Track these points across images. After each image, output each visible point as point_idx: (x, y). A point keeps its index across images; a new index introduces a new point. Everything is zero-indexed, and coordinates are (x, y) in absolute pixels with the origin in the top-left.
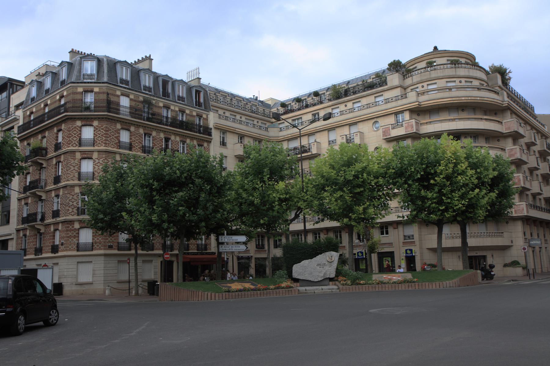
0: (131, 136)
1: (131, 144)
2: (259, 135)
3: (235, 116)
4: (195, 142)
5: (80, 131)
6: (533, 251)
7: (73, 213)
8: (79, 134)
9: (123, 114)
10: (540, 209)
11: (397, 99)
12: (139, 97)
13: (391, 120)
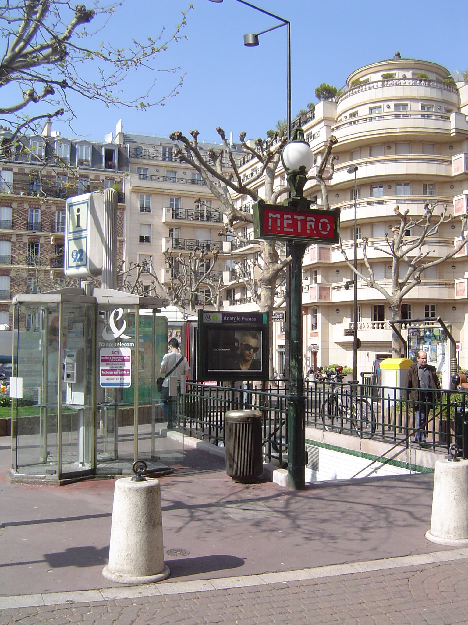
2: (204, 194)
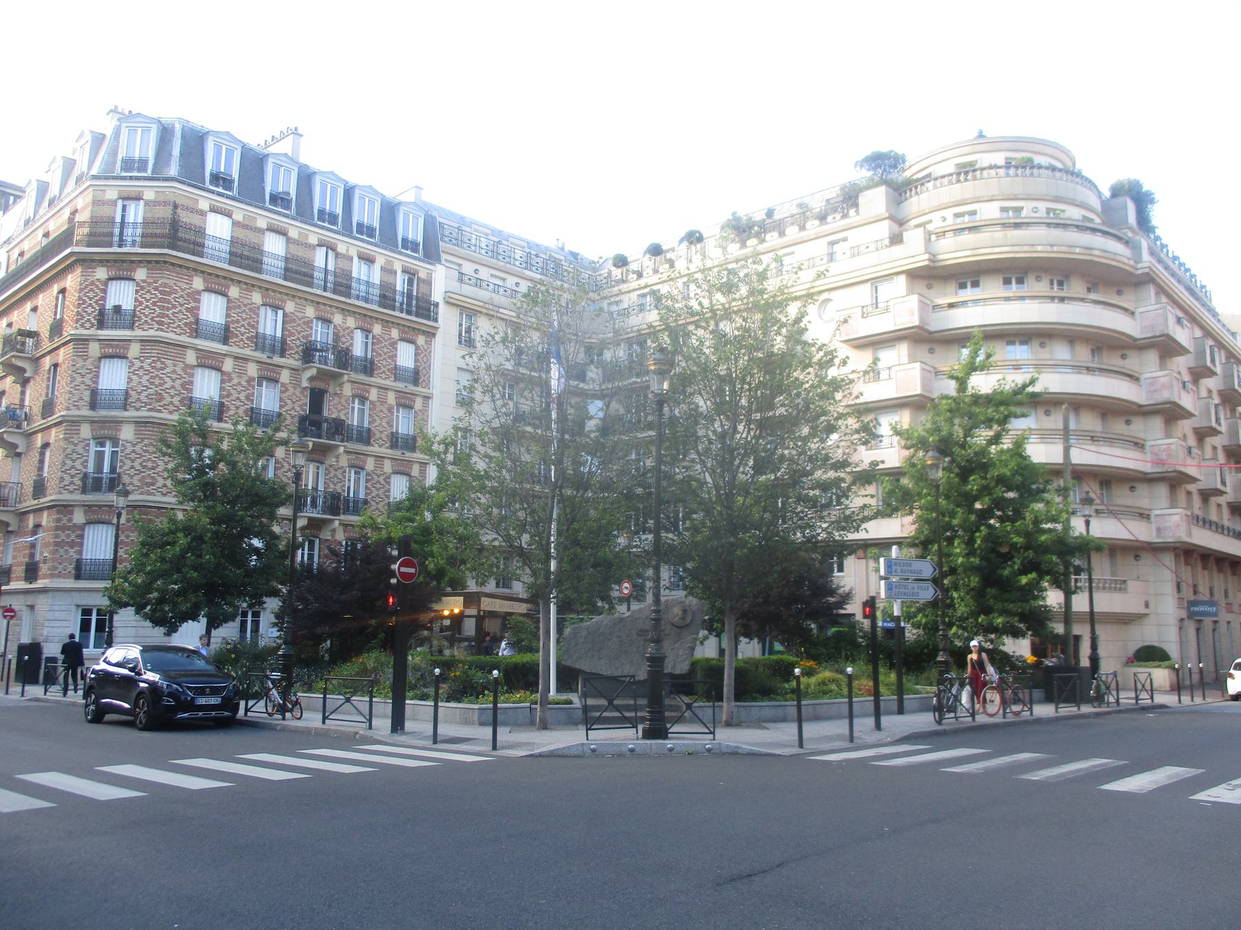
0: (228, 308)
1: (227, 329)
3: (504, 280)
4: (395, 333)
5: (105, 291)
6: (1198, 630)
7: (71, 488)
8: (100, 300)
9: (212, 257)
10: (1219, 528)
11: (879, 246)
12: (197, 200)
13: (863, 294)
